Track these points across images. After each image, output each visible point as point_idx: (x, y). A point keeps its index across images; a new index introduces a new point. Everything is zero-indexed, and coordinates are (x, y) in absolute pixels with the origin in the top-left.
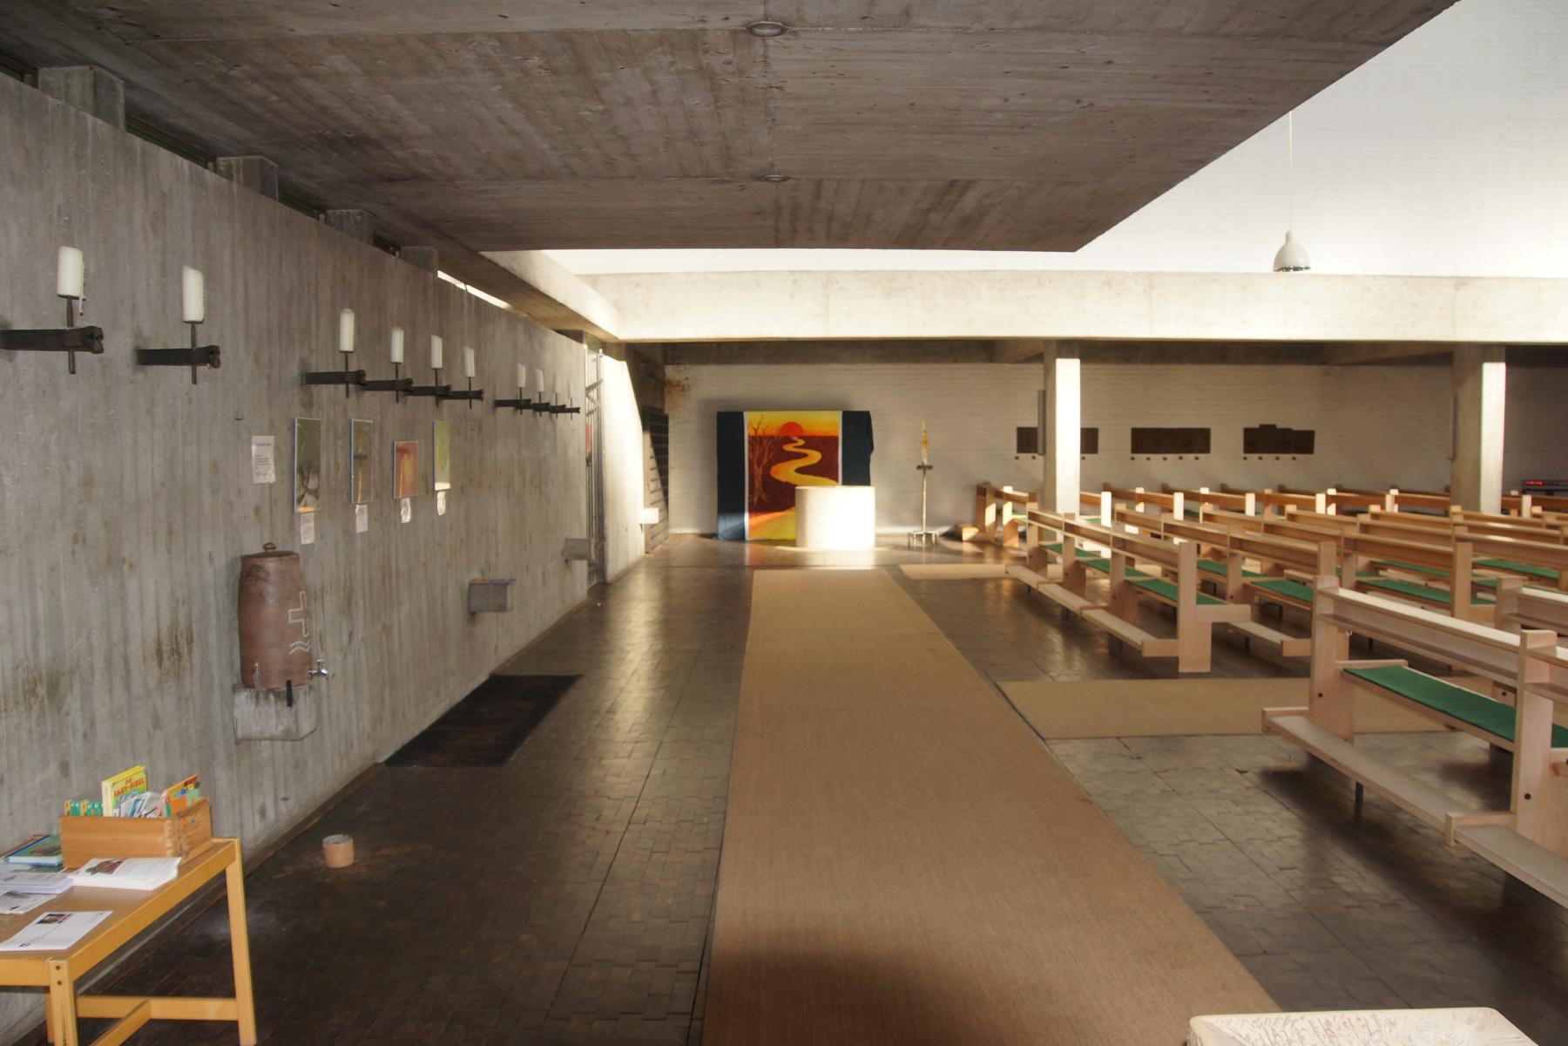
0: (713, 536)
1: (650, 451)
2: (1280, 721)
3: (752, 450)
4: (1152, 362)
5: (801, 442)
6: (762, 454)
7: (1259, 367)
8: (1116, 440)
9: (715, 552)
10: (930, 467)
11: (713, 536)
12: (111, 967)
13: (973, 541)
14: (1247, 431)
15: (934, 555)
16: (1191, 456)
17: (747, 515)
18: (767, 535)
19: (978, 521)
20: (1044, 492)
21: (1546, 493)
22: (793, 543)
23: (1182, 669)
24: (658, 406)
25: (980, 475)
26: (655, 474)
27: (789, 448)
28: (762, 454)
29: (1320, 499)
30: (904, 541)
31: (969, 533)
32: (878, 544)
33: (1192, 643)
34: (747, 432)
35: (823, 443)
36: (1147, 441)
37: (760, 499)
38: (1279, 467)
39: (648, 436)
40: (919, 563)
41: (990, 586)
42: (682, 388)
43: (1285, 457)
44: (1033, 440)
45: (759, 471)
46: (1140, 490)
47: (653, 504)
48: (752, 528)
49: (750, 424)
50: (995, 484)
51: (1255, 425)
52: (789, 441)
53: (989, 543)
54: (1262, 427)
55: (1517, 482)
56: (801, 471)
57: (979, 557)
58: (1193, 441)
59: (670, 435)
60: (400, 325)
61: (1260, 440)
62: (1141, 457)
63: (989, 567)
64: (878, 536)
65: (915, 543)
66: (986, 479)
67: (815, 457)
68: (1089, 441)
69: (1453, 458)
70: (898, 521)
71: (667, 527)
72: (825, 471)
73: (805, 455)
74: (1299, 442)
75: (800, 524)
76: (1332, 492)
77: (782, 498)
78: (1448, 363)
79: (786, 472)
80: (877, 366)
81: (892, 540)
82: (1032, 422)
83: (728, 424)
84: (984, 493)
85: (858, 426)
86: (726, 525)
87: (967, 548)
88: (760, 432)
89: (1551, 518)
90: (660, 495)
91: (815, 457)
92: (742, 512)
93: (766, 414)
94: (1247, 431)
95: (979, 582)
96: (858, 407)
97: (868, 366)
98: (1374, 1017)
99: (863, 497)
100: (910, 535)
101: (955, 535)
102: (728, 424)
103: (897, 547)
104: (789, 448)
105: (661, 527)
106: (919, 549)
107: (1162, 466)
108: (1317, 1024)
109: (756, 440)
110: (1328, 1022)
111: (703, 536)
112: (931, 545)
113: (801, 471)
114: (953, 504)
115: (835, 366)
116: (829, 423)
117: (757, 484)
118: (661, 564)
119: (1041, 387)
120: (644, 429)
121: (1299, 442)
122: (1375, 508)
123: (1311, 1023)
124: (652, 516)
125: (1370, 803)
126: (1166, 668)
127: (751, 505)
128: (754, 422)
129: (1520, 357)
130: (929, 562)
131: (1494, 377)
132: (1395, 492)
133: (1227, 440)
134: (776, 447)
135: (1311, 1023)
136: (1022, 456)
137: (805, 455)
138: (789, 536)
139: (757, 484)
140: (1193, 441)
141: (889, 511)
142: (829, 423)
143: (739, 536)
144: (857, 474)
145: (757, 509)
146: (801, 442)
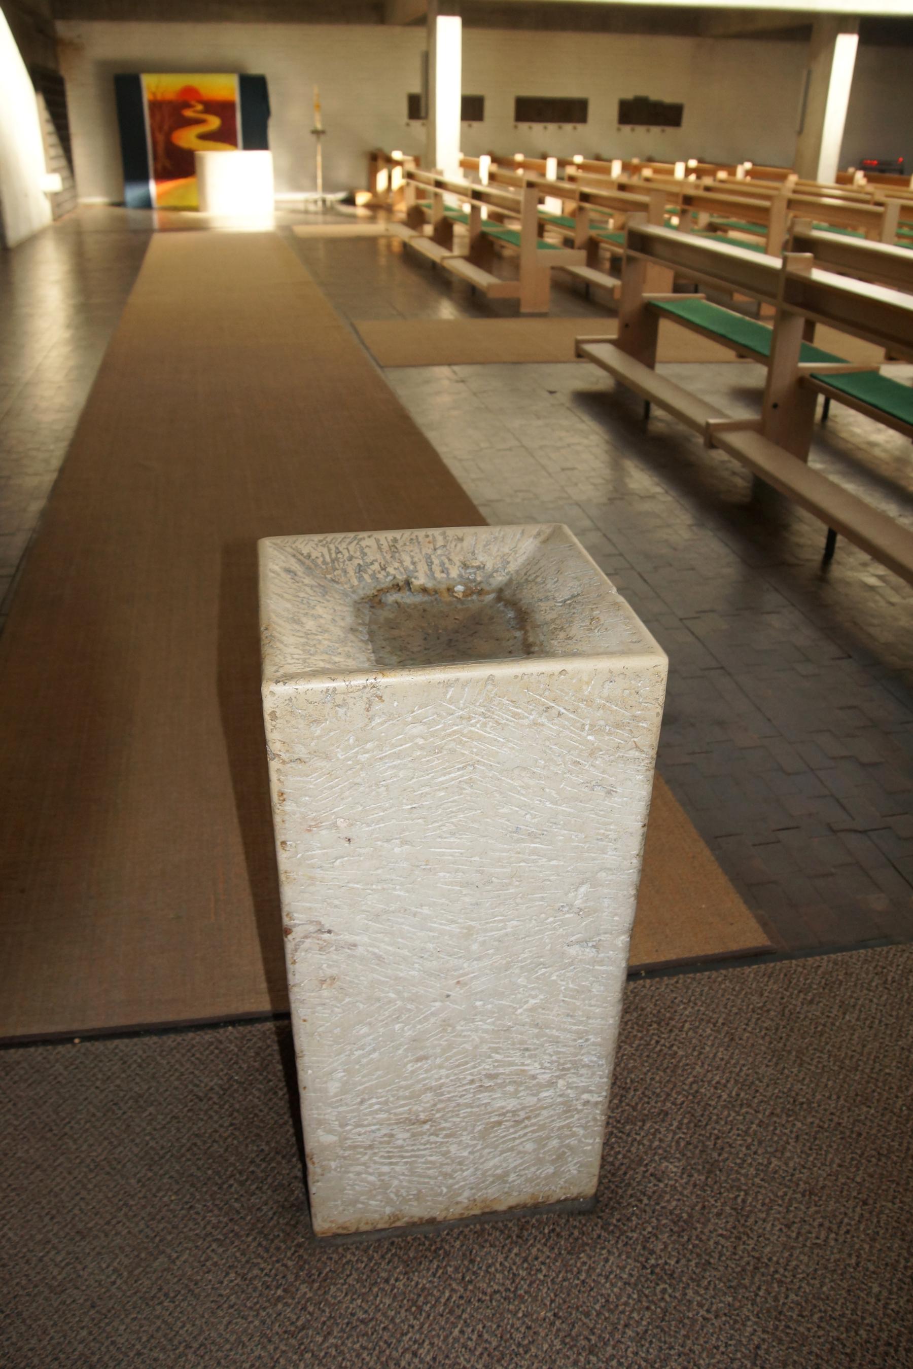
0: (121, 204)
1: (46, 115)
2: (590, 348)
3: (152, 115)
5: (200, 107)
8: (499, 108)
9: (123, 220)
10: (323, 132)
13: (368, 206)
15: (329, 218)
18: (173, 202)
19: (371, 186)
20: (425, 157)
21: (879, 171)
22: (195, 209)
23: (524, 310)
24: (51, 65)
25: (375, 141)
26: (54, 139)
27: (189, 113)
29: (679, 170)
30: (301, 207)
31: (362, 198)
32: (277, 209)
33: (534, 288)
34: (146, 97)
35: (222, 108)
36: (530, 110)
38: (648, 137)
39: (41, 99)
40: (316, 223)
41: (382, 242)
42: (76, 47)
43: (655, 130)
44: (419, 107)
45: (161, 138)
46: (519, 157)
47: (54, 171)
48: (160, 196)
50: (386, 150)
52: (188, 106)
53: (379, 207)
55: (849, 158)
56: (204, 137)
57: (372, 219)
58: (571, 111)
60: (809, 270)
61: (636, 112)
62: (524, 126)
63: (379, 227)
64: (277, 202)
65: (312, 208)
67: (214, 123)
68: (472, 108)
69: (800, 132)
70: (297, 186)
71: (75, 196)
72: (224, 137)
74: (664, 115)
75: (201, 190)
76: (693, 163)
77: (183, 166)
78: (807, 34)
79: (187, 138)
81: (290, 206)
82: (416, 89)
84: (377, 159)
85: (255, 89)
86: (133, 193)
87: (361, 212)
88: (159, 97)
89: (871, 188)
90: (63, 162)
91: (214, 123)
95: (371, 241)
96: (255, 69)
98: (444, 534)
99: (261, 159)
100: (306, 201)
101: (350, 201)
102: (123, 87)
103: (294, 211)
104: (189, 113)
105: (67, 196)
106: (316, 213)
107: (541, 134)
108: (383, 541)
109: (155, 105)
110: (395, 540)
112: (328, 209)
114: (348, 169)
116: (226, 87)
118: (72, 232)
119: (423, 47)
121: (664, 115)
122: (722, 175)
123: (377, 541)
124: (55, 183)
125: (656, 418)
126: (510, 308)
127: (156, 171)
128: (152, 86)
129: (875, 31)
130: (325, 223)
131: (846, 47)
132: (748, 165)
133: (602, 111)
134: (175, 112)
135: (377, 541)
138: (193, 202)
140: (571, 111)
141: (293, 177)
142: (226, 87)
143: (146, 204)
144: (256, 139)
145: (162, 176)
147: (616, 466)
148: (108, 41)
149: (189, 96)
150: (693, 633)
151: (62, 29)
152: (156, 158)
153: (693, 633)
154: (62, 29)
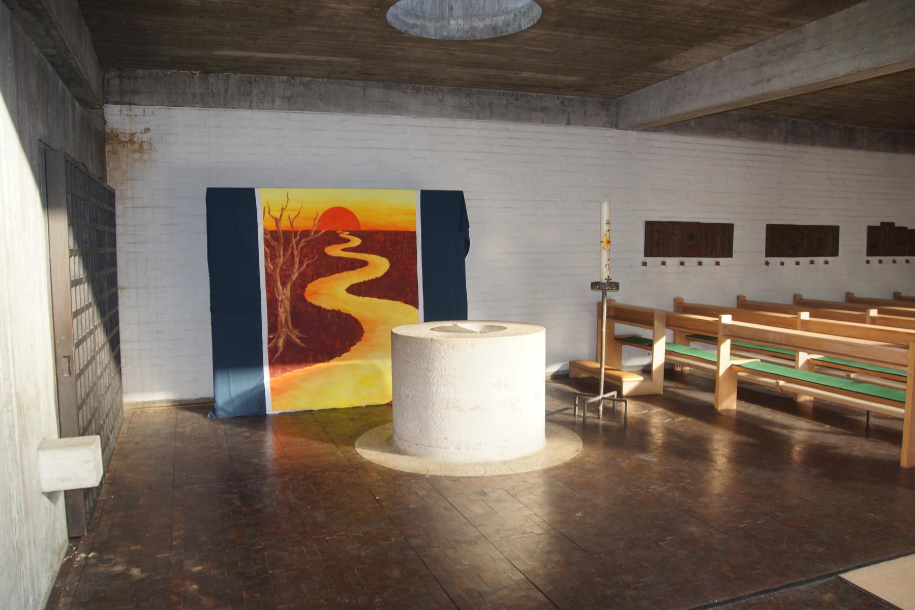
3: (272, 256)
4: (786, 142)
5: (356, 242)
6: (290, 262)
7: (881, 154)
11: (205, 407)
12: (492, 72)
14: (871, 229)
16: (820, 260)
17: (266, 369)
27: (335, 251)
28: (290, 262)
34: (262, 224)
37: (289, 343)
39: (61, 224)
42: (138, 146)
45: (284, 294)
49: (267, 210)
51: (877, 223)
54: (882, 223)
59: (317, 405)
66: (852, 291)
67: (379, 266)
73: (364, 264)
80: (460, 123)
83: (230, 212)
85: (446, 213)
86: (231, 390)
88: (285, 224)
91: (379, 266)
92: (260, 365)
93: (295, 193)
94: (871, 229)
97: (446, 122)
102: (230, 212)
104: (335, 251)
111: (184, 405)
113: (355, 290)
115: (398, 119)
116: (401, 209)
117: (283, 314)
120: (48, 203)
127: (273, 351)
128: (274, 206)
134: (316, 247)
136: (650, 260)
137: (364, 264)
139: (283, 314)
142: (401, 209)
145: (287, 357)
146: (356, 242)
147: (109, 362)
148: (185, 147)
149: (338, 221)
150: (87, 366)
151: (116, 117)
152: (273, 329)
153: (87, 366)
154: (116, 117)
